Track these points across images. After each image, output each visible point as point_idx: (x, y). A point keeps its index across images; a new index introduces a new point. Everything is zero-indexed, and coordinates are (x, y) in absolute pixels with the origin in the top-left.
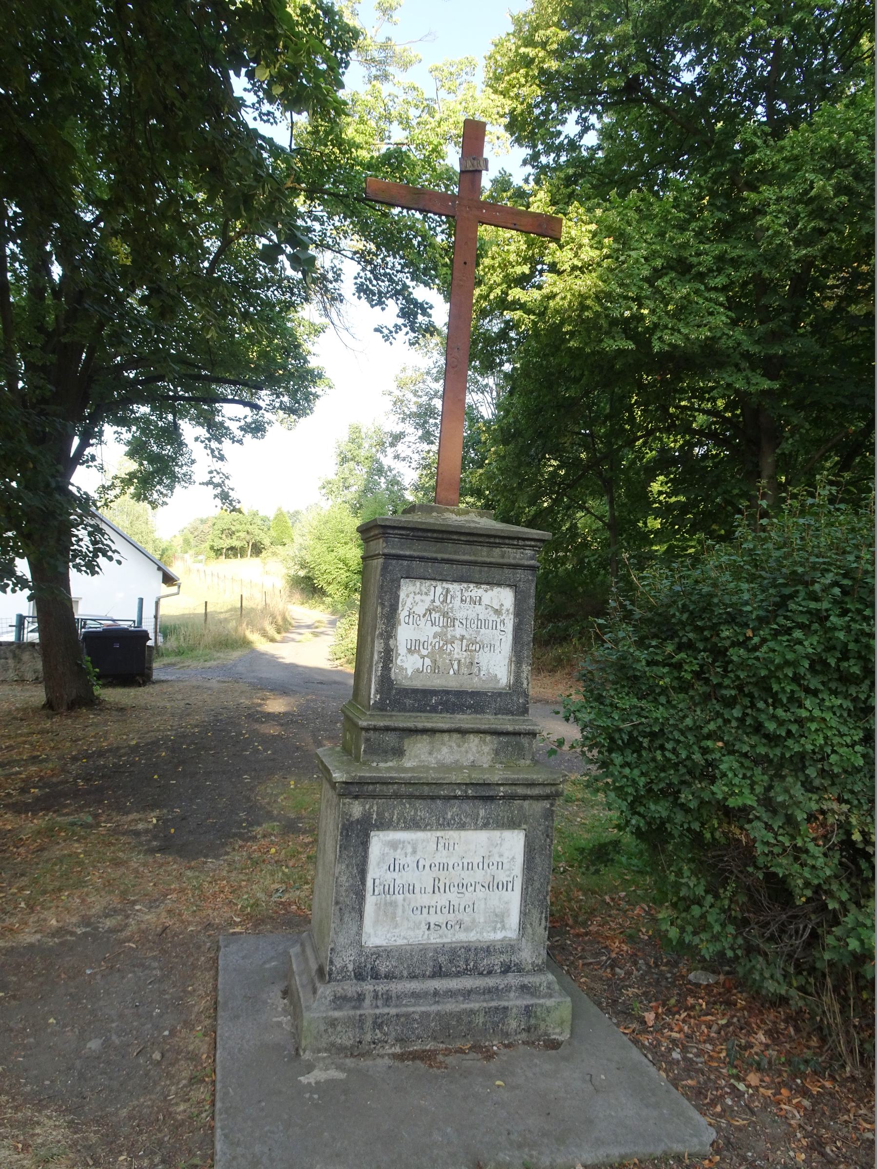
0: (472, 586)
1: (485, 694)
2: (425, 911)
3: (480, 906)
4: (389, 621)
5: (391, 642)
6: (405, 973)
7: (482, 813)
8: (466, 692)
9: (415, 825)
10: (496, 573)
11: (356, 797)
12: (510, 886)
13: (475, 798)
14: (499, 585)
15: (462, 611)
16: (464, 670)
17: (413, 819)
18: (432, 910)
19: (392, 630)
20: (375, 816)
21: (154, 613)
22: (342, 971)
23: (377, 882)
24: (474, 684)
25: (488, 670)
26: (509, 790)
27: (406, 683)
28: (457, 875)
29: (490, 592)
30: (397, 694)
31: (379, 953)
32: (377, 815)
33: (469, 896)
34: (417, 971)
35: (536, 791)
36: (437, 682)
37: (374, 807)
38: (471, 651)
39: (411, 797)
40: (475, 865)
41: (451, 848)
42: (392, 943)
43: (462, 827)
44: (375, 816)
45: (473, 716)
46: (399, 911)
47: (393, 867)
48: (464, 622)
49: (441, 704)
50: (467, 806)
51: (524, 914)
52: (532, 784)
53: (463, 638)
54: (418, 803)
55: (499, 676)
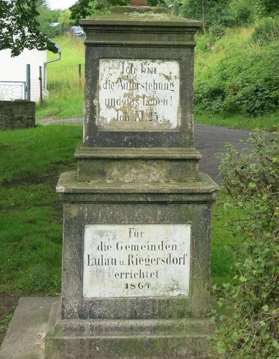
0: (149, 61)
1: (162, 133)
2: (129, 276)
3: (161, 274)
4: (92, 87)
5: (95, 101)
6: (112, 316)
7: (159, 212)
8: (148, 133)
9: (113, 221)
10: (167, 52)
11: (73, 203)
12: (182, 261)
13: (154, 203)
14: (169, 59)
15: (142, 78)
16: (147, 118)
17: (112, 217)
18: (129, 276)
19: (95, 93)
20: (86, 215)
21: (38, 75)
22: (70, 313)
23: (91, 257)
24: (154, 127)
25: (163, 117)
26: (177, 198)
27: (107, 128)
28: (143, 254)
29: (162, 64)
30: (100, 135)
31: (94, 302)
32: (88, 214)
33: (153, 268)
34: (120, 314)
35: (196, 198)
36: (127, 127)
37: (86, 209)
38: (151, 105)
39: (110, 203)
40: (140, 247)
41: (140, 236)
42: (102, 296)
43: (146, 222)
44: (86, 215)
45: (154, 149)
46: (106, 276)
47: (101, 247)
48: (145, 85)
49: (130, 141)
50: (149, 208)
51: (192, 279)
52: (192, 194)
53: (144, 96)
54: (115, 207)
55: (171, 122)
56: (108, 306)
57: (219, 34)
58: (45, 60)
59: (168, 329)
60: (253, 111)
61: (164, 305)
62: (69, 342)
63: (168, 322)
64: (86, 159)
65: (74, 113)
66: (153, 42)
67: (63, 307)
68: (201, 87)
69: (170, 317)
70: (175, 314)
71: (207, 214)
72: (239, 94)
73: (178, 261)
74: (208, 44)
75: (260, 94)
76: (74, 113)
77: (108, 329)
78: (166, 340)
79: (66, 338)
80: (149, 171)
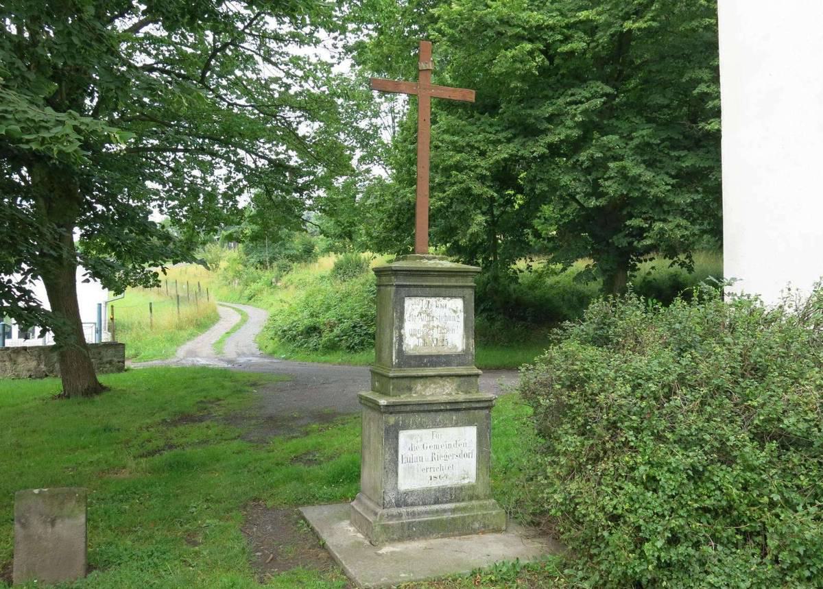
5: (402, 331)
7: (454, 418)
9: (421, 426)
10: (454, 291)
11: (391, 413)
13: (451, 410)
14: (455, 297)
15: (437, 312)
16: (440, 344)
18: (429, 470)
24: (445, 350)
26: (468, 405)
28: (443, 452)
31: (406, 493)
36: (425, 351)
37: (401, 417)
43: (445, 426)
46: (416, 472)
50: (447, 415)
51: (478, 469)
52: (479, 401)
53: (438, 327)
54: (422, 415)
56: (418, 495)
57: (285, 269)
58: (106, 300)
59: (464, 509)
60: (353, 347)
61: (458, 492)
62: (392, 526)
63: (463, 504)
64: (397, 378)
65: (155, 356)
66: (445, 284)
67: (384, 499)
68: (294, 324)
69: (463, 500)
70: (467, 498)
71: (488, 417)
72: (337, 331)
73: (467, 455)
74: (274, 280)
75: (358, 330)
76: (155, 356)
77: (420, 514)
78: (463, 518)
79: (391, 523)
80: (444, 386)
